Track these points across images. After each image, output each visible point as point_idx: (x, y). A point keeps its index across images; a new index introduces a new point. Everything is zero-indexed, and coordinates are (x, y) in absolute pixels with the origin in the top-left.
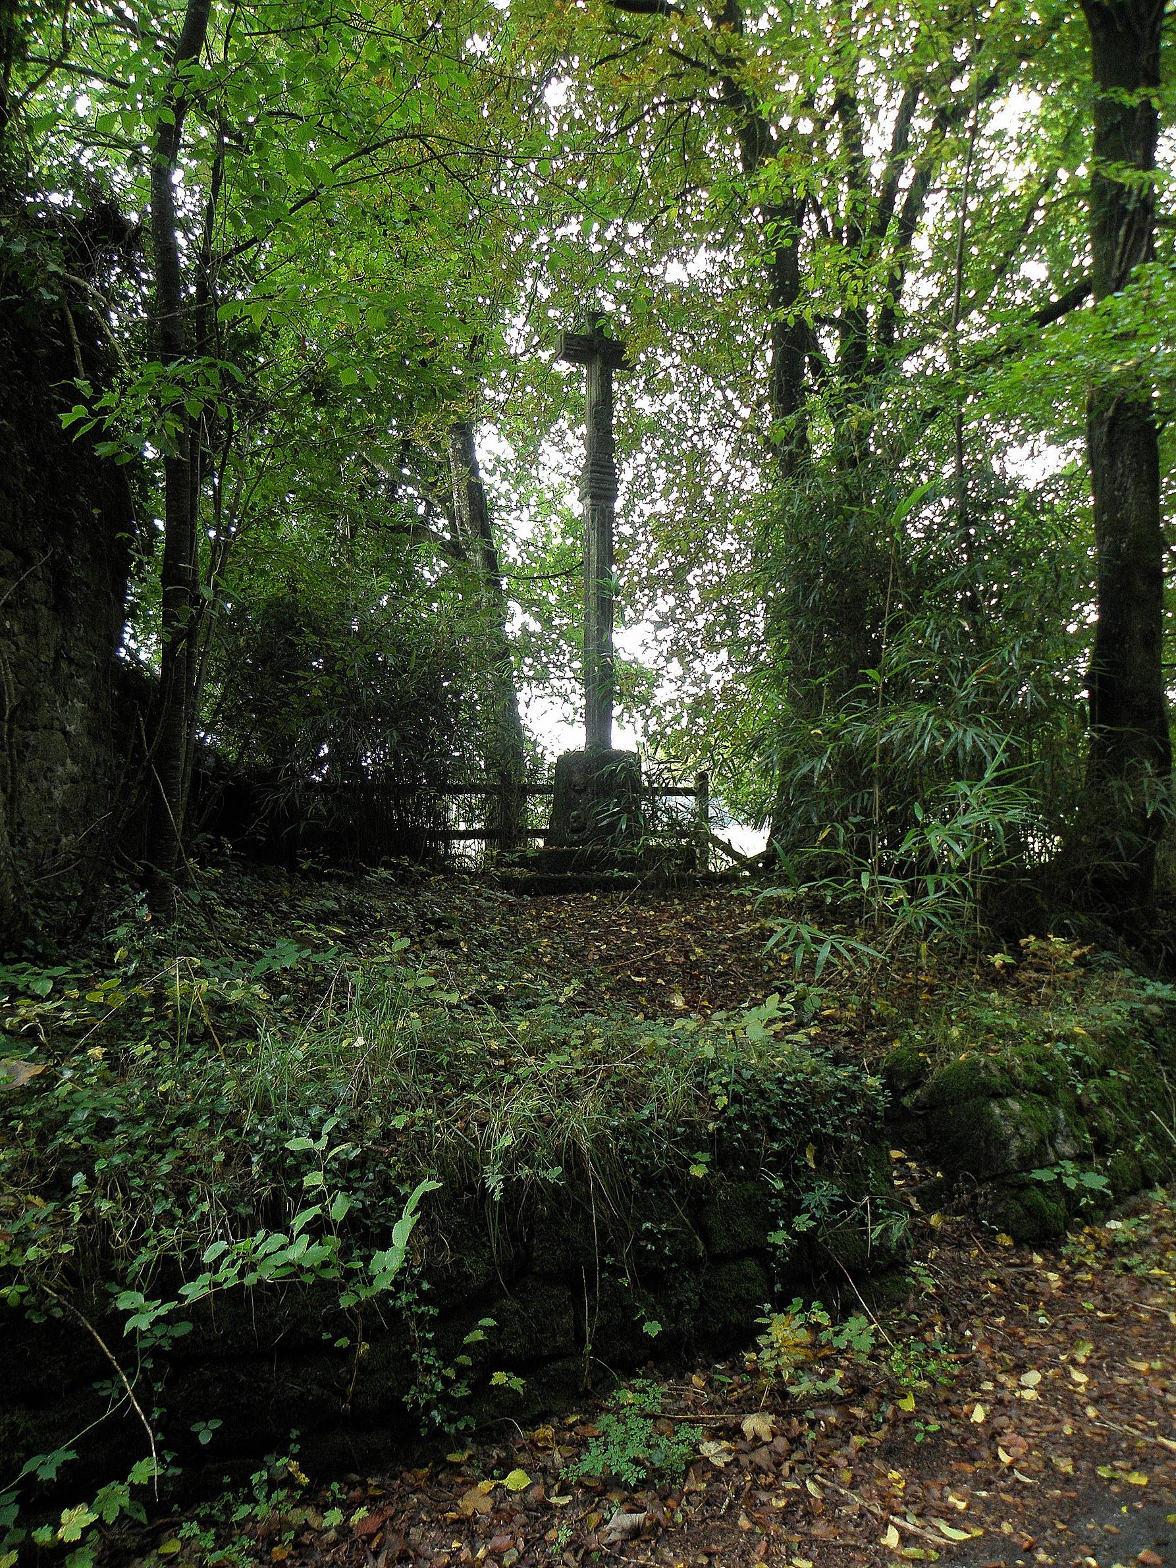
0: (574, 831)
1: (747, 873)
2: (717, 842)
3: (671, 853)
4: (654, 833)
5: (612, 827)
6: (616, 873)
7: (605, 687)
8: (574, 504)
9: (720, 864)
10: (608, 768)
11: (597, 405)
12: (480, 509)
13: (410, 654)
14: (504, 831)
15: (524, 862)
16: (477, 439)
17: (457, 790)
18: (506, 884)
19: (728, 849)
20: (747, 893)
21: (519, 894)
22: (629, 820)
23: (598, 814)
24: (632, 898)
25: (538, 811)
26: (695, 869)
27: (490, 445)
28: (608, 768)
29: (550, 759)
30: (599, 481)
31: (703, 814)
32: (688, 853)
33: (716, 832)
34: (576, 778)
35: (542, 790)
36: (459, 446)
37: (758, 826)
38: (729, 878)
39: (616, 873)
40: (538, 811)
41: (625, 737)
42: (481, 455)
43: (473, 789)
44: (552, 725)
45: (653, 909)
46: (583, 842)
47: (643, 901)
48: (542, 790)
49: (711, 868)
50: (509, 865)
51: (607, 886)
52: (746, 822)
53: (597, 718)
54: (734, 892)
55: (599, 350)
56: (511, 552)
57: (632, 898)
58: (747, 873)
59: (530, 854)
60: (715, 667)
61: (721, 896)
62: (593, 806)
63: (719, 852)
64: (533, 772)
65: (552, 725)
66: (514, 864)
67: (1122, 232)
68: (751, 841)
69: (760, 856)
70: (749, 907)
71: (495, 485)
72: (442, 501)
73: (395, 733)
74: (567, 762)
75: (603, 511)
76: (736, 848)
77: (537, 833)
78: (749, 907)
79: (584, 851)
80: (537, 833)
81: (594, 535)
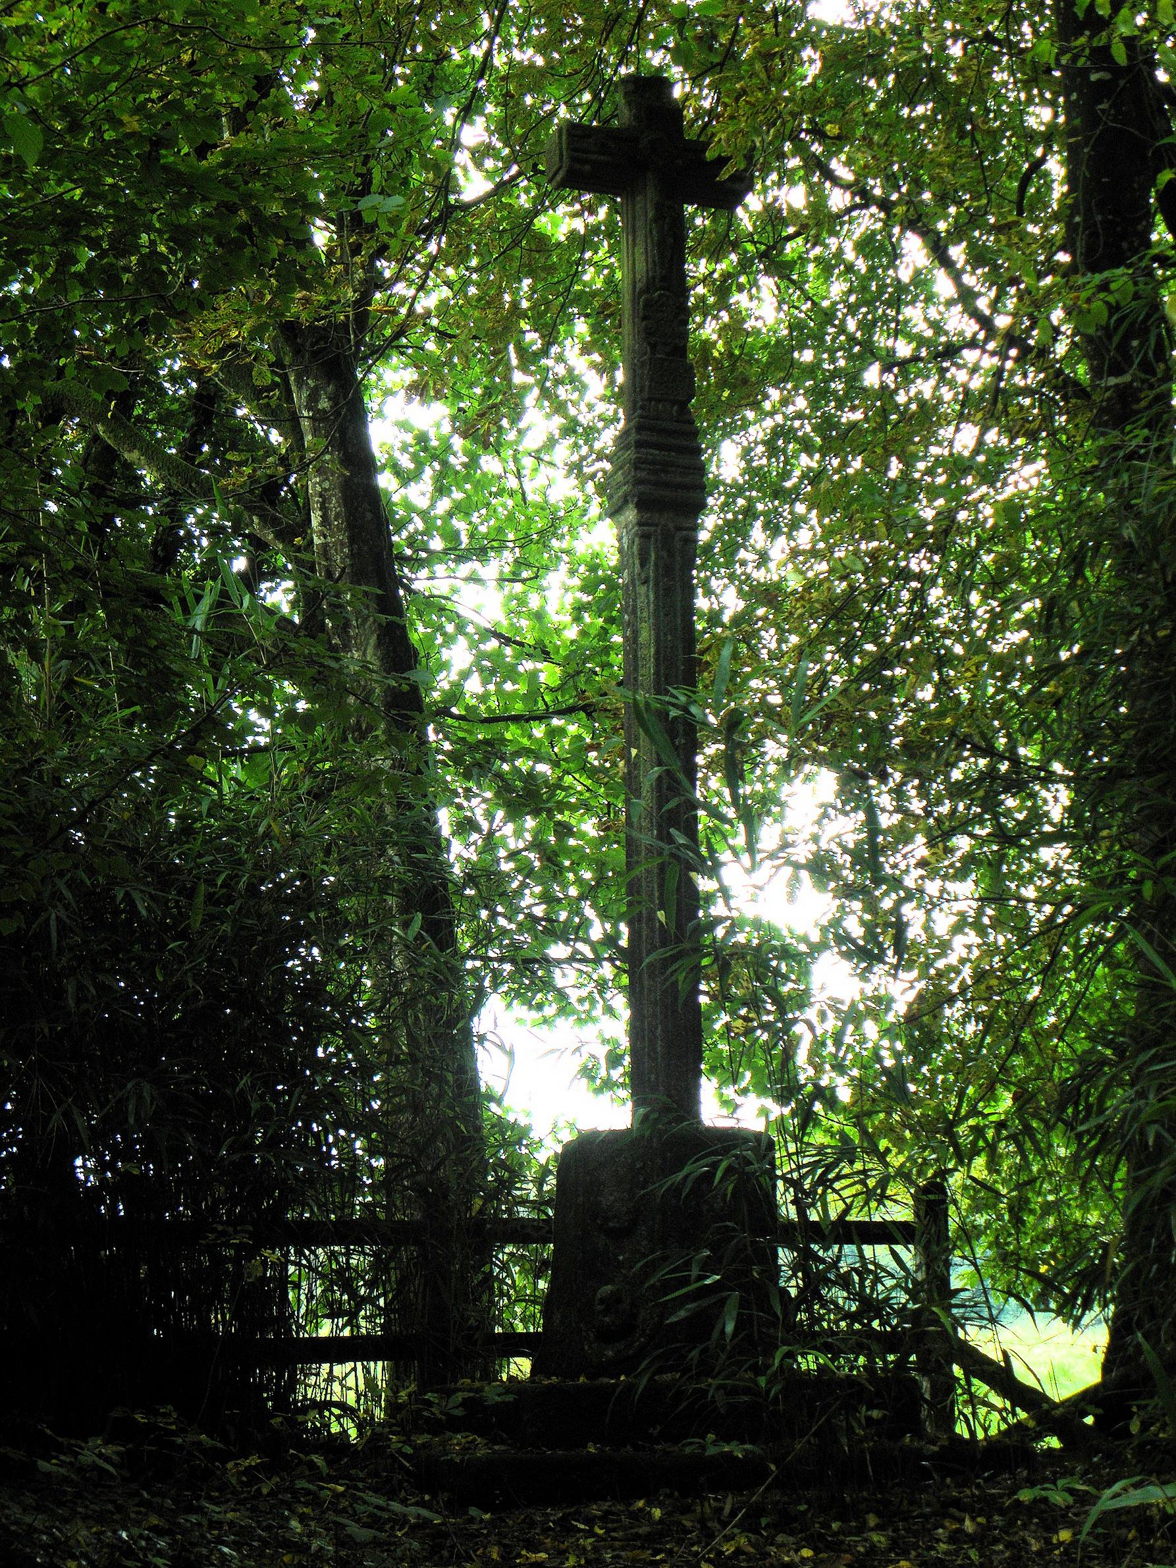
0: (606, 1336)
1: (1054, 1442)
2: (978, 1365)
3: (852, 1392)
4: (810, 1339)
5: (703, 1324)
6: (713, 1447)
7: (684, 991)
8: (602, 539)
9: (986, 1417)
10: (696, 1168)
11: (647, 289)
12: (372, 544)
13: (191, 894)
14: (432, 1336)
15: (477, 1416)
16: (372, 401)
17: (308, 1235)
18: (428, 1477)
19: (1000, 1376)
20: (1059, 1498)
21: (457, 1506)
22: (743, 1304)
23: (667, 1287)
24: (756, 1512)
25: (520, 1292)
26: (919, 1433)
27: (399, 414)
28: (696, 1168)
29: (546, 1151)
30: (660, 478)
31: (934, 1285)
32: (895, 1392)
33: (976, 1336)
34: (609, 1198)
35: (521, 1233)
36: (324, 404)
37: (1070, 1311)
38: (1010, 1452)
39: (713, 1447)
40: (520, 1292)
41: (729, 1106)
42: (384, 435)
43: (348, 1233)
44: (549, 1073)
45: (811, 1543)
46: (626, 1364)
47: (786, 1522)
48: (521, 1233)
49: (961, 1429)
50: (435, 1427)
51: (689, 1481)
52: (1041, 1303)
53: (666, 1056)
54: (1025, 1496)
55: (651, 165)
56: (454, 667)
57: (756, 1512)
58: (1054, 1442)
59: (491, 1395)
60: (947, 913)
61: (988, 1506)
62: (652, 1267)
63: (981, 1388)
64: (505, 1185)
65: (549, 1073)
66: (454, 1424)
67: (682, 1314)
68: (1062, 1354)
69: (1088, 1398)
70: (1065, 1535)
71: (409, 496)
72: (285, 535)
73: (147, 1090)
74: (585, 1158)
75: (667, 539)
76: (1021, 1375)
77: (515, 1344)
78: (1065, 1535)
79: (630, 1388)
80: (515, 1344)
81: (646, 596)
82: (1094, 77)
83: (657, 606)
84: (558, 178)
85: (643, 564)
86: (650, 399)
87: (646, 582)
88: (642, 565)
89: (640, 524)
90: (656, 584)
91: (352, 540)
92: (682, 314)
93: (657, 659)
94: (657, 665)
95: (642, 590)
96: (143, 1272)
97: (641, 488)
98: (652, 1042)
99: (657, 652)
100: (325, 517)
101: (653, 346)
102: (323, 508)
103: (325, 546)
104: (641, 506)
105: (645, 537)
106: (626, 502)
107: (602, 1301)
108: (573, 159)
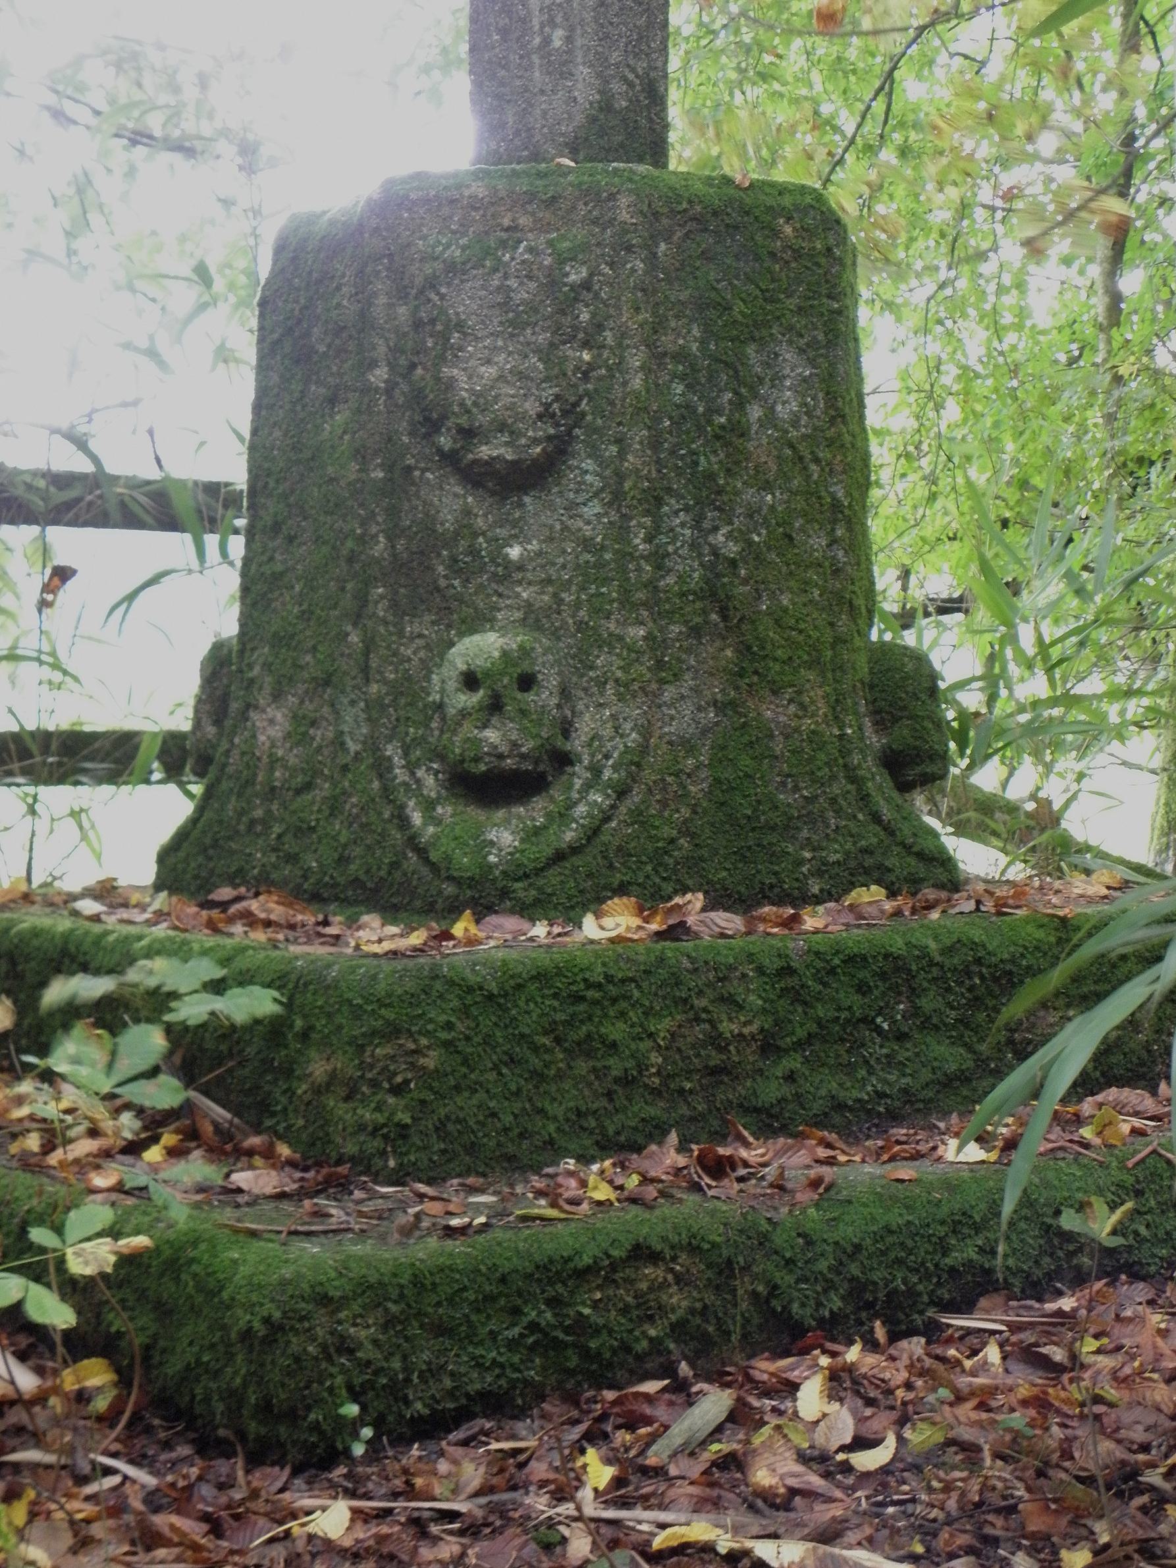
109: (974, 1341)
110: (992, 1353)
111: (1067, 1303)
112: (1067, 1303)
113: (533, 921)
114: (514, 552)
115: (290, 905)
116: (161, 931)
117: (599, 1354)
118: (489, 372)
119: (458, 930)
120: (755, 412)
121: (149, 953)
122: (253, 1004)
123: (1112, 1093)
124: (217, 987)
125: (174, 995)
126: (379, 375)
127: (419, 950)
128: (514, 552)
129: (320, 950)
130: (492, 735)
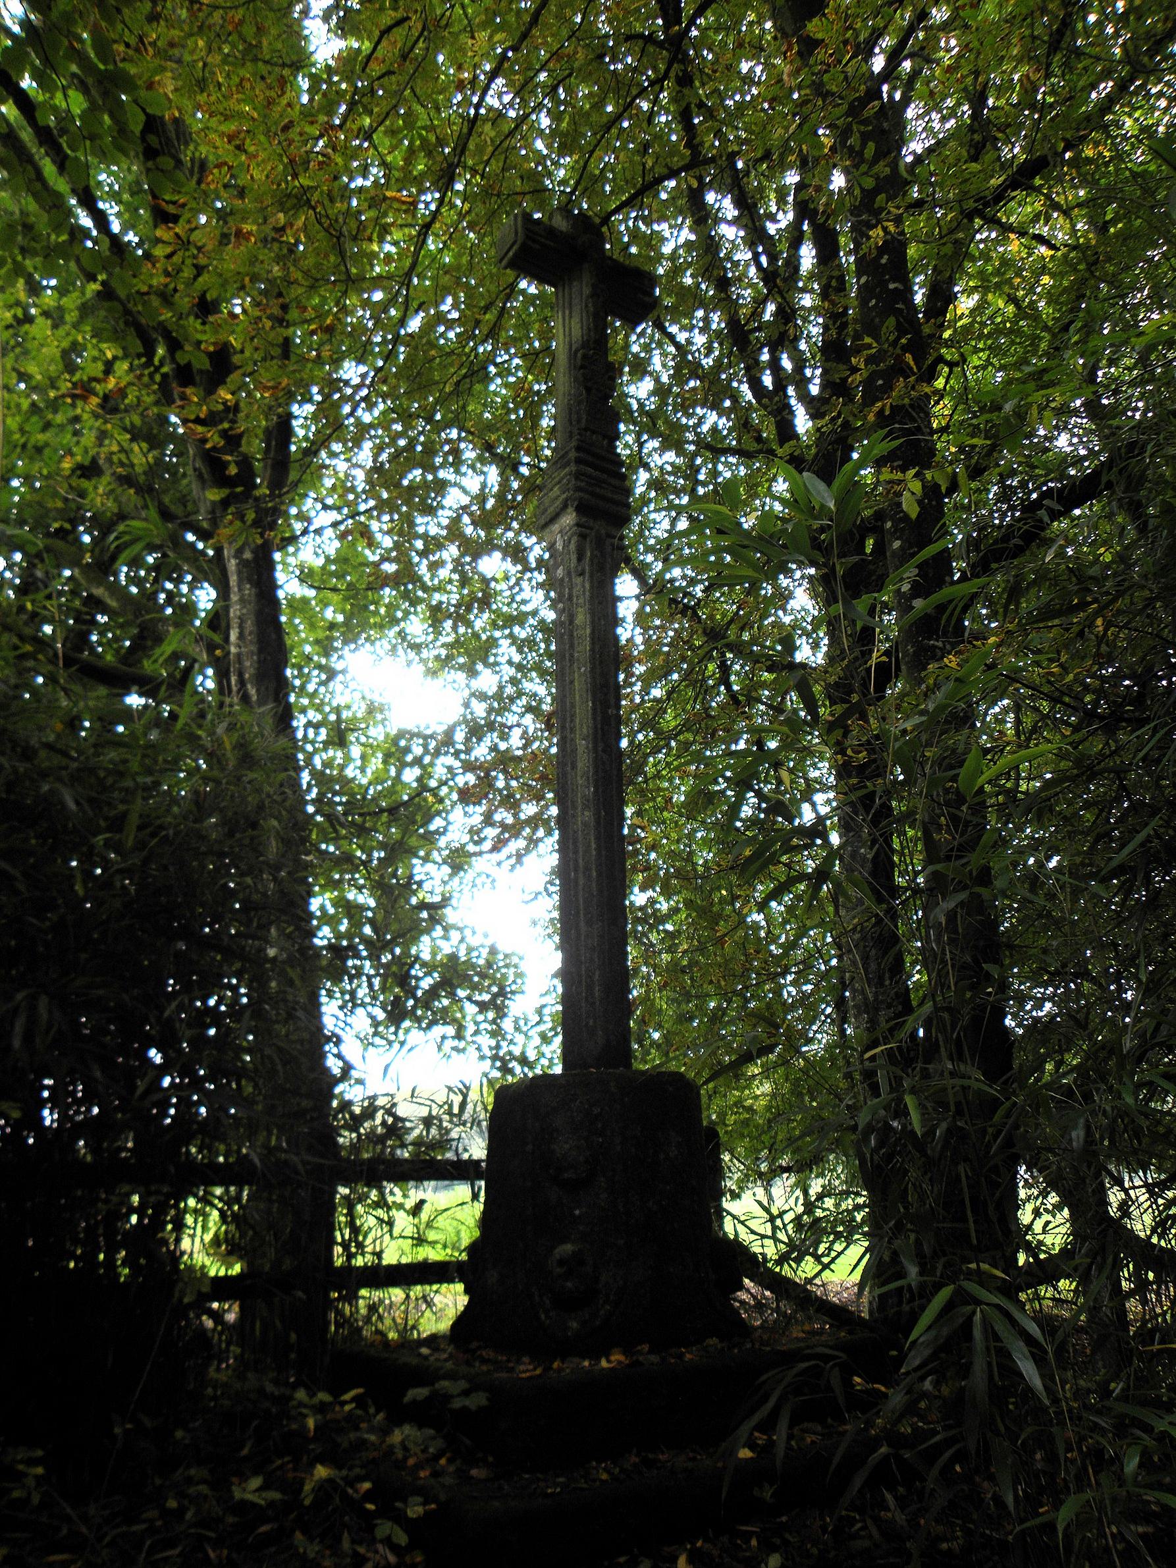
75: (599, 543)
82: (892, 286)
83: (591, 597)
84: (505, 262)
85: (580, 559)
86: (586, 429)
87: (582, 574)
88: (579, 559)
89: (578, 525)
90: (591, 576)
91: (261, 651)
92: (613, 372)
93: (592, 639)
94: (593, 643)
95: (579, 580)
96: (102, 1256)
97: (578, 494)
98: (590, 987)
99: (593, 632)
100: (241, 636)
101: (588, 390)
102: (241, 627)
103: (239, 655)
104: (581, 509)
105: (583, 536)
106: (565, 507)
107: (561, 1262)
108: (527, 237)
109: (747, 1536)
110: (754, 1542)
111: (784, 1519)
112: (784, 1519)
113: (584, 1359)
114: (577, 1212)
115: (572, 355)
116: (449, 1365)
117: (1030, 508)
118: (567, 1146)
119: (555, 1365)
120: (662, 1156)
121: (444, 1378)
122: (478, 1400)
123: (805, 1425)
124: (466, 1393)
125: (452, 1396)
126: (529, 1148)
127: (540, 1376)
128: (577, 1212)
129: (504, 1375)
130: (569, 1284)
